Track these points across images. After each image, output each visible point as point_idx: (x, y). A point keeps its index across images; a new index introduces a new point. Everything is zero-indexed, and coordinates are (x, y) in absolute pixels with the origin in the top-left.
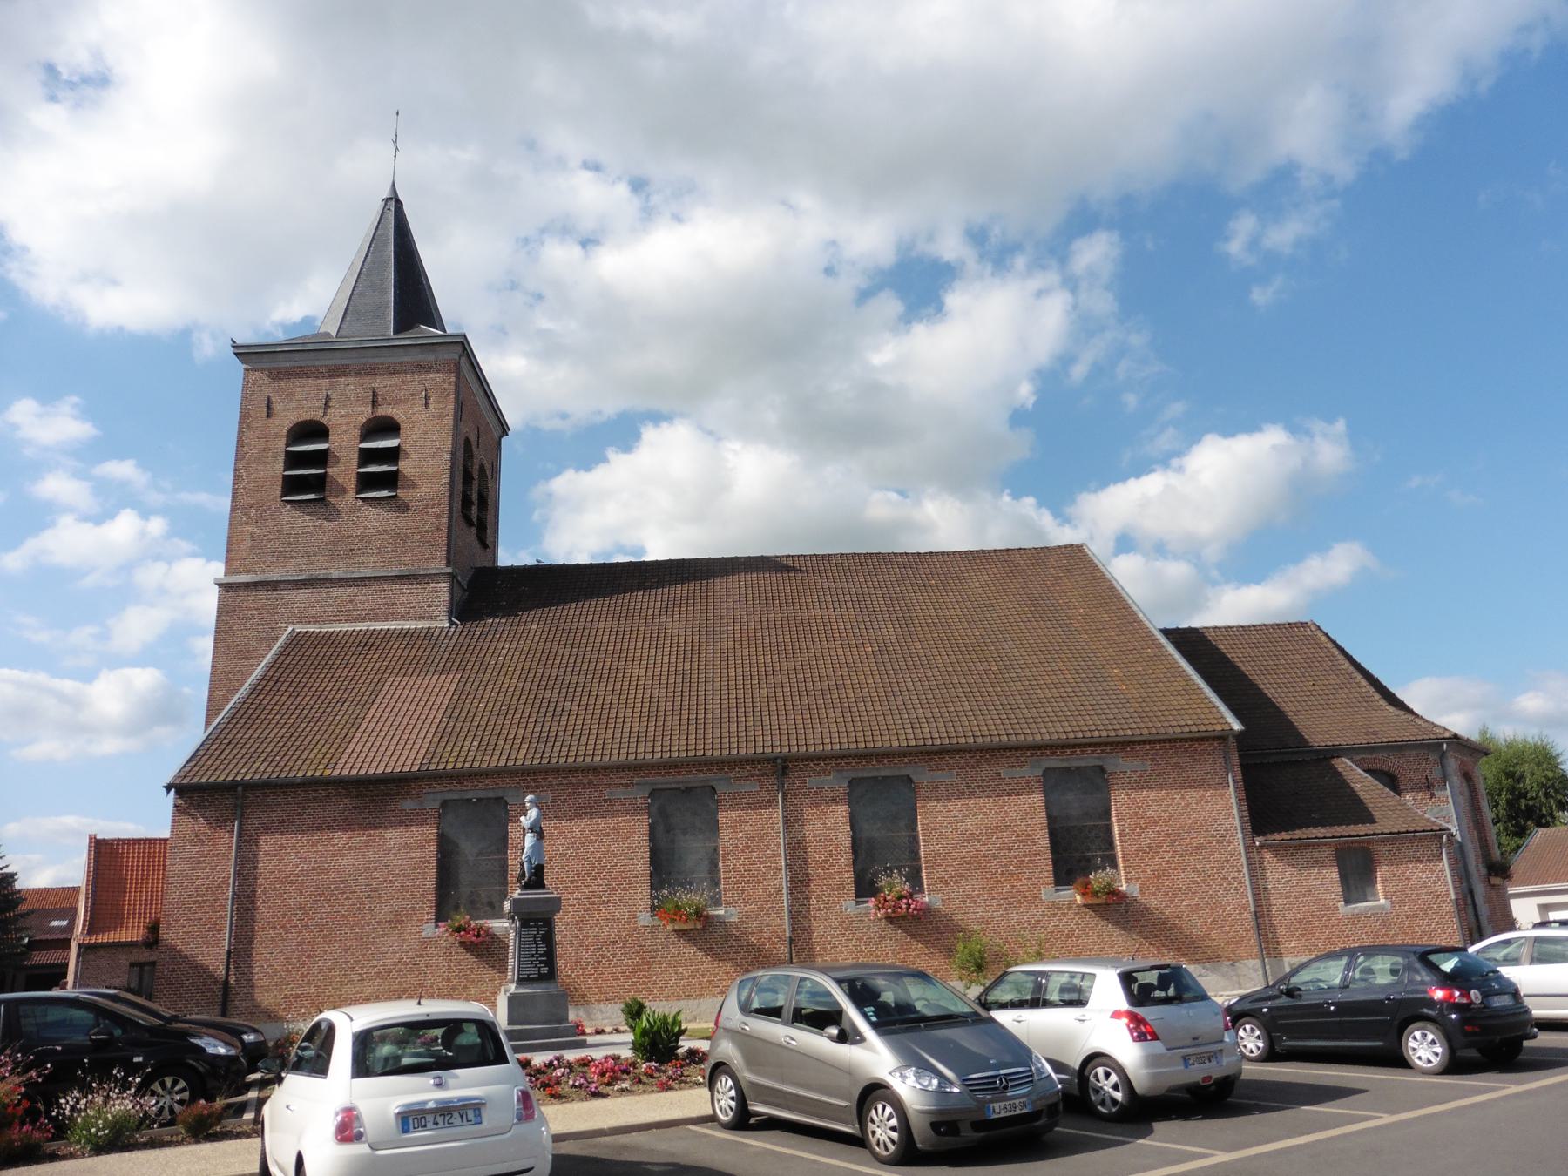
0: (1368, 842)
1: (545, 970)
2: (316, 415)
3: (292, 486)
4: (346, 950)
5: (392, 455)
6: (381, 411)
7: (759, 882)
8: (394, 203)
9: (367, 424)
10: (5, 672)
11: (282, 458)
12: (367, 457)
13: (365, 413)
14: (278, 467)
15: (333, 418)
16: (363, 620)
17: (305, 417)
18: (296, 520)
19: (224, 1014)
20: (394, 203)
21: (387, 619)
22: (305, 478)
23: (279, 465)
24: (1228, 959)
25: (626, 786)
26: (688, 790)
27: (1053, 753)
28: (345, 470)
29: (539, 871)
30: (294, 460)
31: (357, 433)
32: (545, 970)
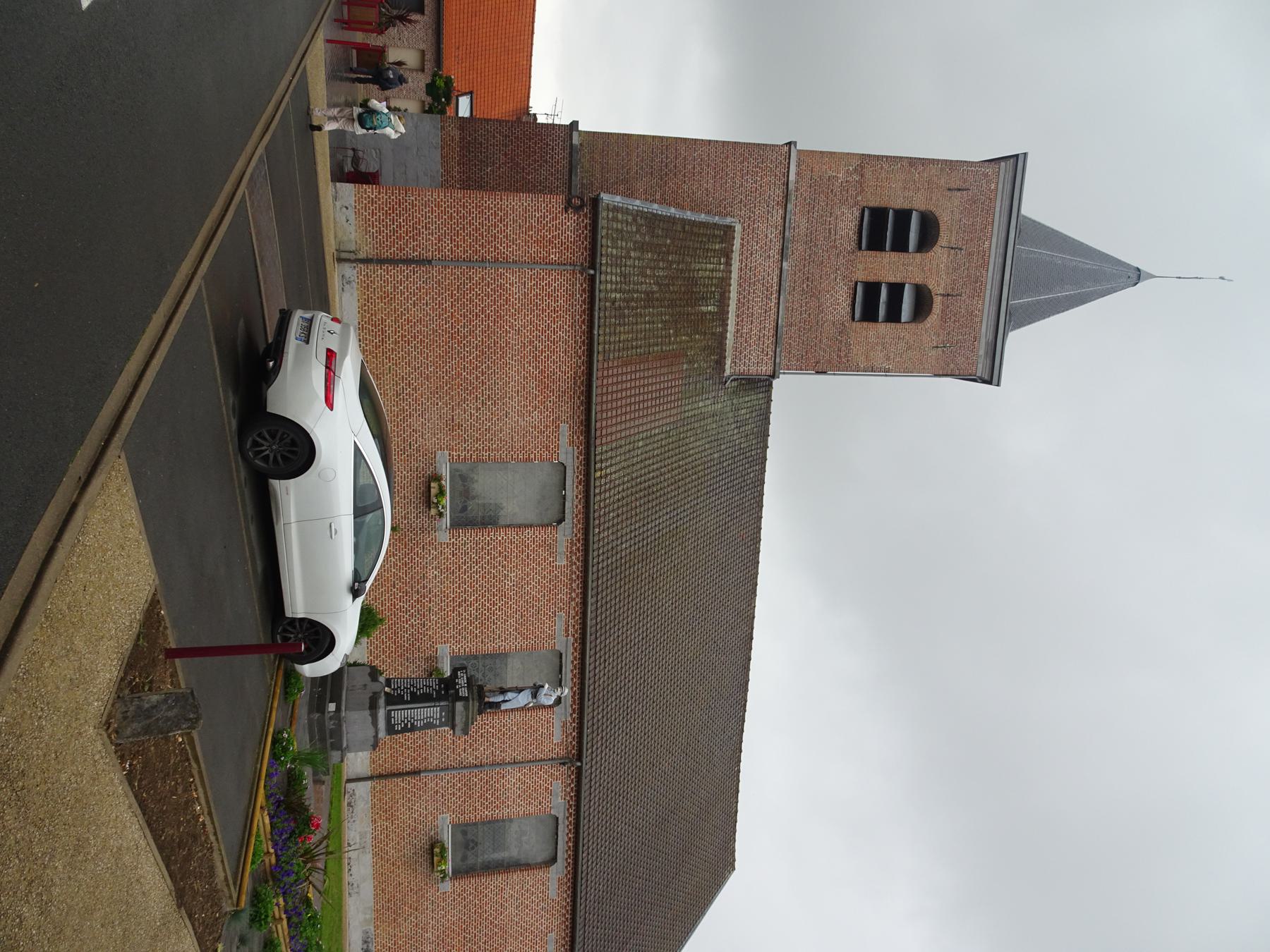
2: (943, 240)
3: (878, 215)
4: (428, 378)
6: (938, 301)
8: (1137, 276)
9: (930, 263)
10: (358, 912)
11: (906, 206)
12: (896, 290)
13: (937, 286)
15: (939, 254)
17: (943, 228)
18: (847, 223)
20: (1137, 276)
22: (884, 229)
23: (899, 203)
25: (567, 630)
28: (887, 267)
29: (488, 521)
30: (903, 216)
31: (919, 280)
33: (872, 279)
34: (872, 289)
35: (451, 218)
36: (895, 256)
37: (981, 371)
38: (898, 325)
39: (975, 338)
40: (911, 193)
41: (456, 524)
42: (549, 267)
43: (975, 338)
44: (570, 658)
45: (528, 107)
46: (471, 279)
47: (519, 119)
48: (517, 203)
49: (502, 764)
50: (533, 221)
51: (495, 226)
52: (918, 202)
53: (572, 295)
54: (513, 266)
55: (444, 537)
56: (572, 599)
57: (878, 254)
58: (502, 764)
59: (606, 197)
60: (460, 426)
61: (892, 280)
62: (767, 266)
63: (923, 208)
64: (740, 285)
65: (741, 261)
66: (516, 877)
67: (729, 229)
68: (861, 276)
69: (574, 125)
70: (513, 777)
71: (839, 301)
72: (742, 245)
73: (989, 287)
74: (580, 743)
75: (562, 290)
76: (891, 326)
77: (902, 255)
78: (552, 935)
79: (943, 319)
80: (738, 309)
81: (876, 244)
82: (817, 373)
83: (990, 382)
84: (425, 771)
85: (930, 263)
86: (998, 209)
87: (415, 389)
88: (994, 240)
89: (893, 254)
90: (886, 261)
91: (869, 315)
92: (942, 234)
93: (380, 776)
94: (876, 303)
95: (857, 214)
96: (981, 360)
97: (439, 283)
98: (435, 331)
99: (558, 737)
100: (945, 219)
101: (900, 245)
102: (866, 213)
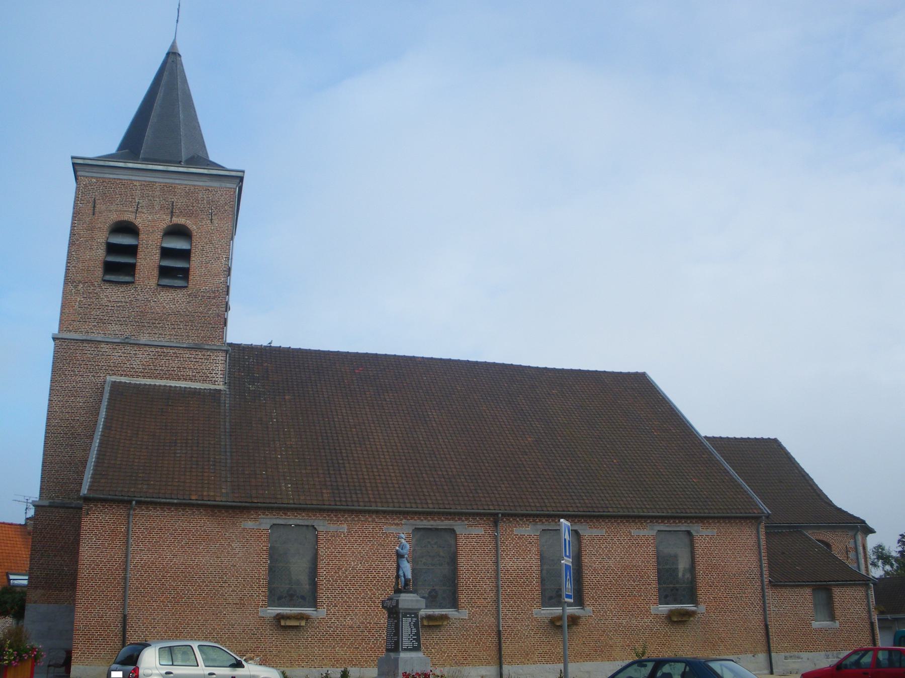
0: (830, 585)
1: (416, 644)
2: (128, 217)
3: (109, 268)
5: (185, 255)
6: (176, 220)
7: (482, 594)
8: (173, 56)
9: (152, 210)
11: (104, 247)
12: (166, 253)
13: (165, 221)
14: (100, 253)
16: (162, 378)
18: (113, 295)
19: (833, 618)
20: (173, 56)
21: (179, 379)
22: (119, 264)
24: (751, 652)
25: (397, 524)
26: (437, 529)
27: (662, 522)
28: (148, 261)
30: (112, 249)
32: (416, 644)
33: (156, 273)
34: (164, 272)
35: (95, 600)
36: (141, 255)
37: (233, 185)
38: (193, 251)
39: (206, 190)
40: (95, 244)
41: (314, 604)
42: (131, 532)
43: (206, 190)
44: (418, 522)
45: (20, 525)
46: (137, 588)
47: (29, 533)
48: (87, 552)
49: (497, 571)
50: (97, 543)
51: (101, 569)
52: (102, 237)
53: (150, 516)
54: (130, 558)
55: (322, 612)
56: (373, 521)
57: (138, 268)
58: (497, 571)
59: (84, 491)
60: (241, 599)
61: (157, 256)
62: (141, 357)
63: (106, 234)
64: (156, 377)
65: (138, 376)
66: (586, 560)
67: (114, 384)
68: (153, 282)
69: (54, 339)
70: (508, 563)
71: (171, 300)
72: (126, 375)
73: (168, 181)
74: (484, 515)
75: (145, 522)
76: (193, 258)
77: (140, 249)
78: (634, 532)
79: (189, 215)
80: (173, 379)
81: (130, 269)
82: (228, 294)
83: (241, 179)
84: (498, 626)
85: (152, 210)
86: (111, 176)
87: (214, 629)
88: (133, 178)
89: (139, 256)
90: (143, 262)
91: (185, 273)
92: (126, 218)
93: (500, 658)
94: (175, 269)
95: (107, 285)
96: (223, 185)
97: (139, 610)
98: (173, 614)
99: (480, 531)
100: (114, 217)
101: (132, 251)
102: (108, 277)
